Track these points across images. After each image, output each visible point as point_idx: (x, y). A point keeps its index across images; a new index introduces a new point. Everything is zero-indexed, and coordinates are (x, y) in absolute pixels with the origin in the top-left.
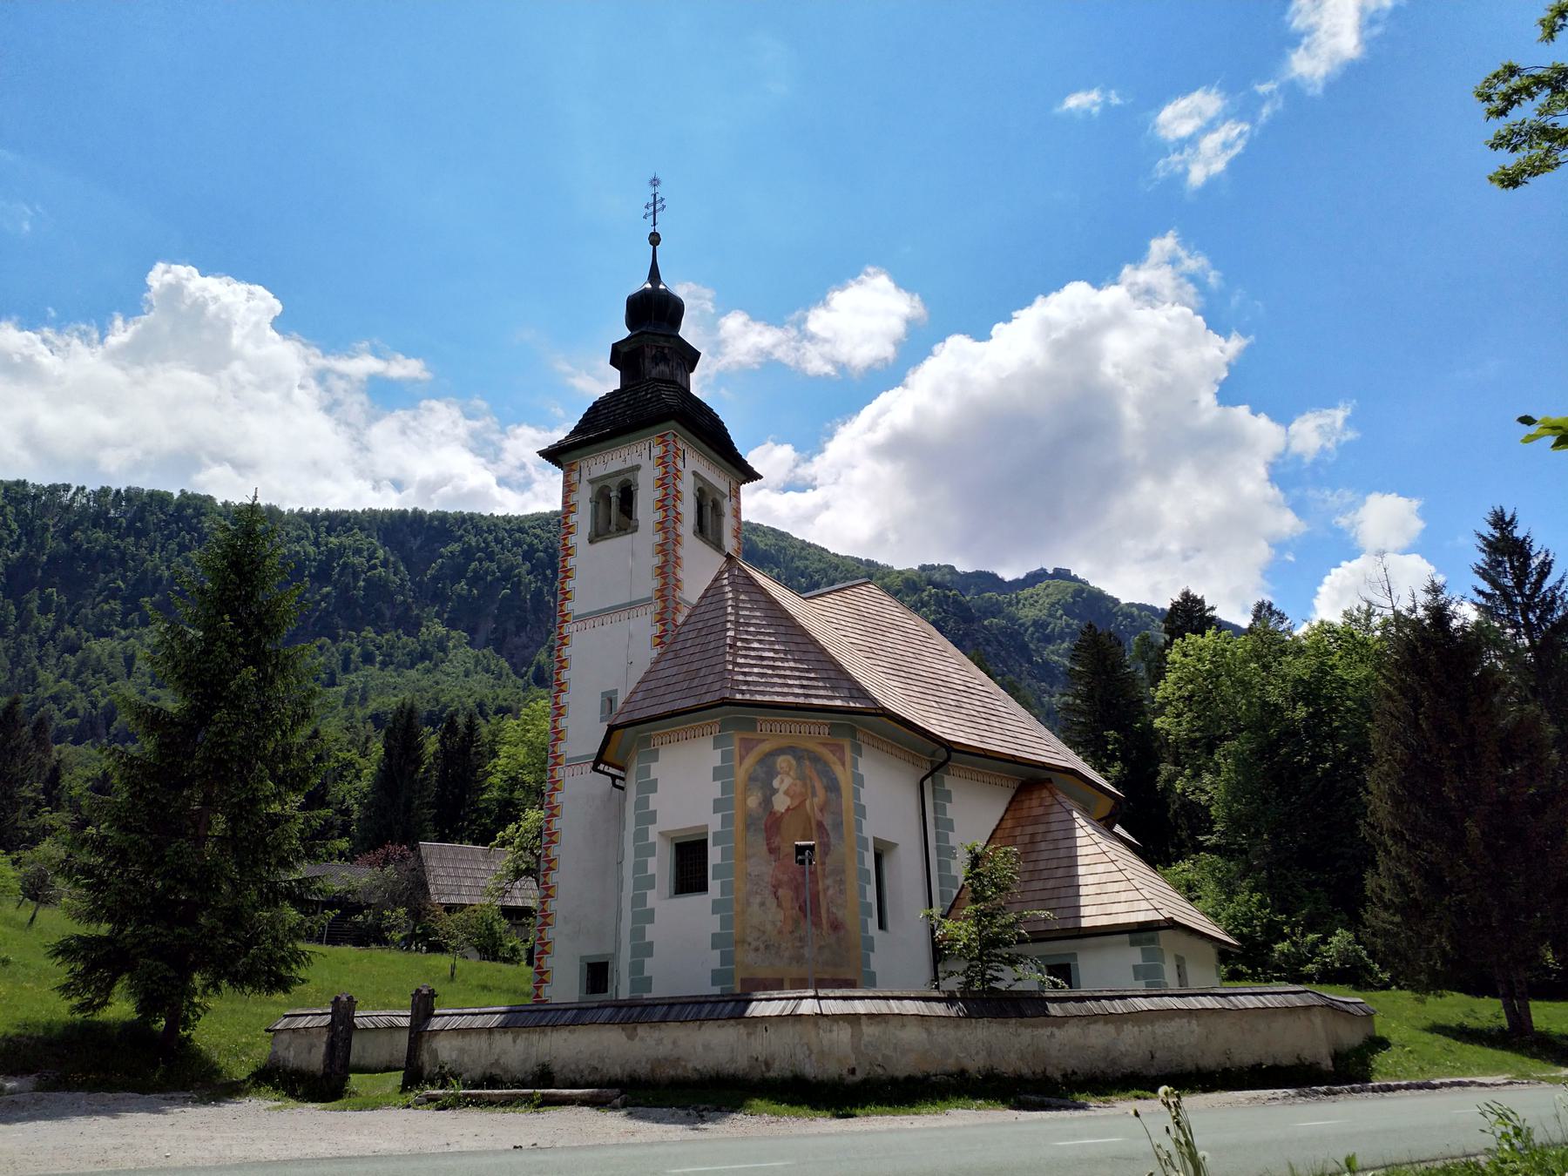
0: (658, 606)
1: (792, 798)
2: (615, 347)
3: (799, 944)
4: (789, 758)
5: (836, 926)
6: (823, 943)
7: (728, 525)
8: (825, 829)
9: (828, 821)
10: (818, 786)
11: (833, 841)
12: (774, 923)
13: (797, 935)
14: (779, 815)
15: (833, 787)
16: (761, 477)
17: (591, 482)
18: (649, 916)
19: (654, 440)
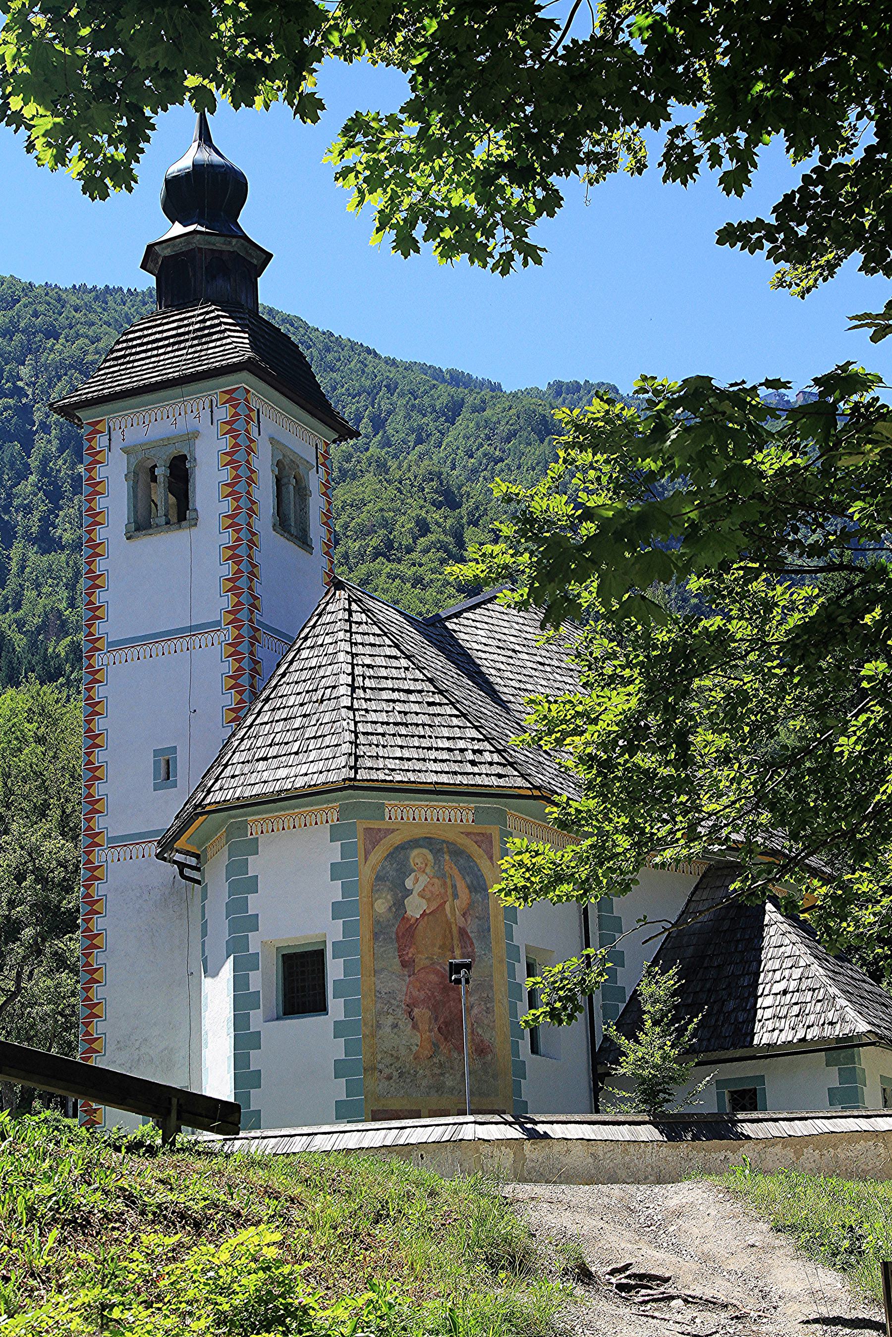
1: (428, 900)
2: (150, 247)
3: (438, 1071)
4: (425, 851)
9: (472, 928)
10: (461, 886)
17: (125, 450)
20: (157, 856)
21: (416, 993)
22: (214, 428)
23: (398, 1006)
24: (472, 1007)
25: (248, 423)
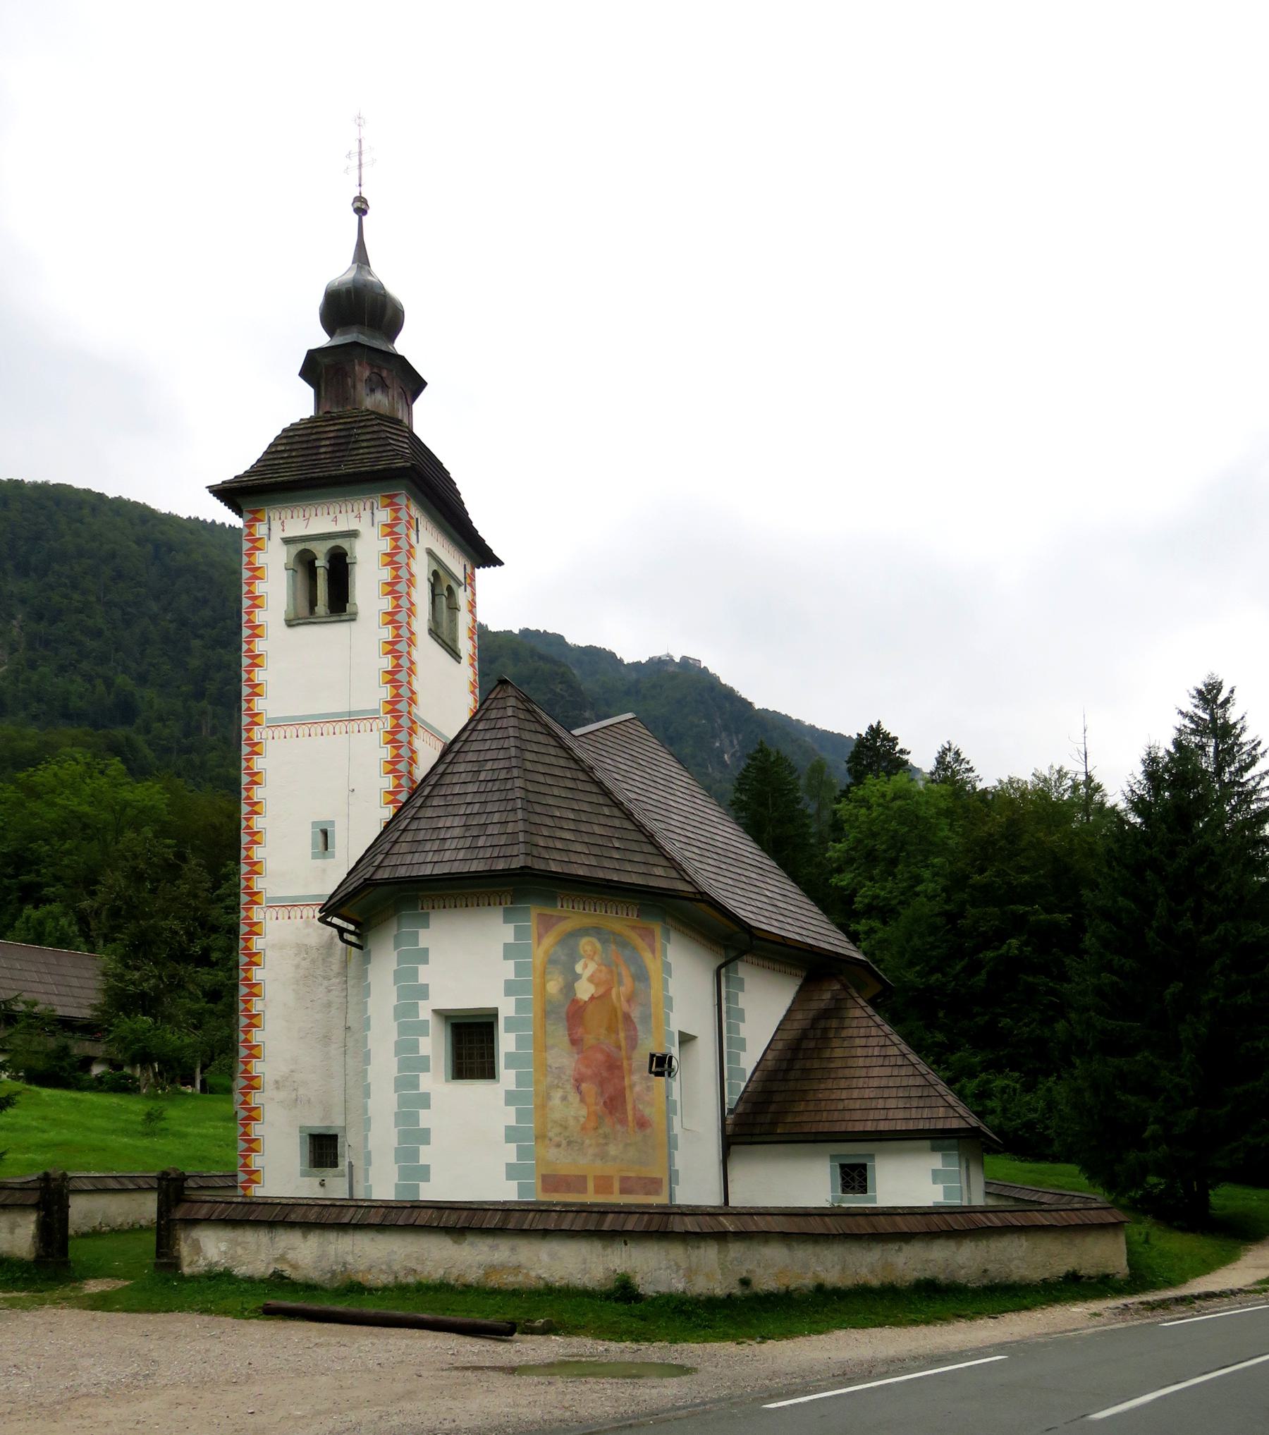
0: (389, 723)
4: (594, 940)
5: (642, 1124)
7: (464, 619)
8: (632, 1021)
9: (635, 1014)
11: (641, 1034)
12: (576, 1118)
13: (601, 1131)
14: (581, 1004)
15: (641, 976)
16: (500, 563)
18: (425, 1101)
19: (378, 500)
20: (319, 919)
21: (583, 1070)
23: (567, 1080)
25: (408, 529)
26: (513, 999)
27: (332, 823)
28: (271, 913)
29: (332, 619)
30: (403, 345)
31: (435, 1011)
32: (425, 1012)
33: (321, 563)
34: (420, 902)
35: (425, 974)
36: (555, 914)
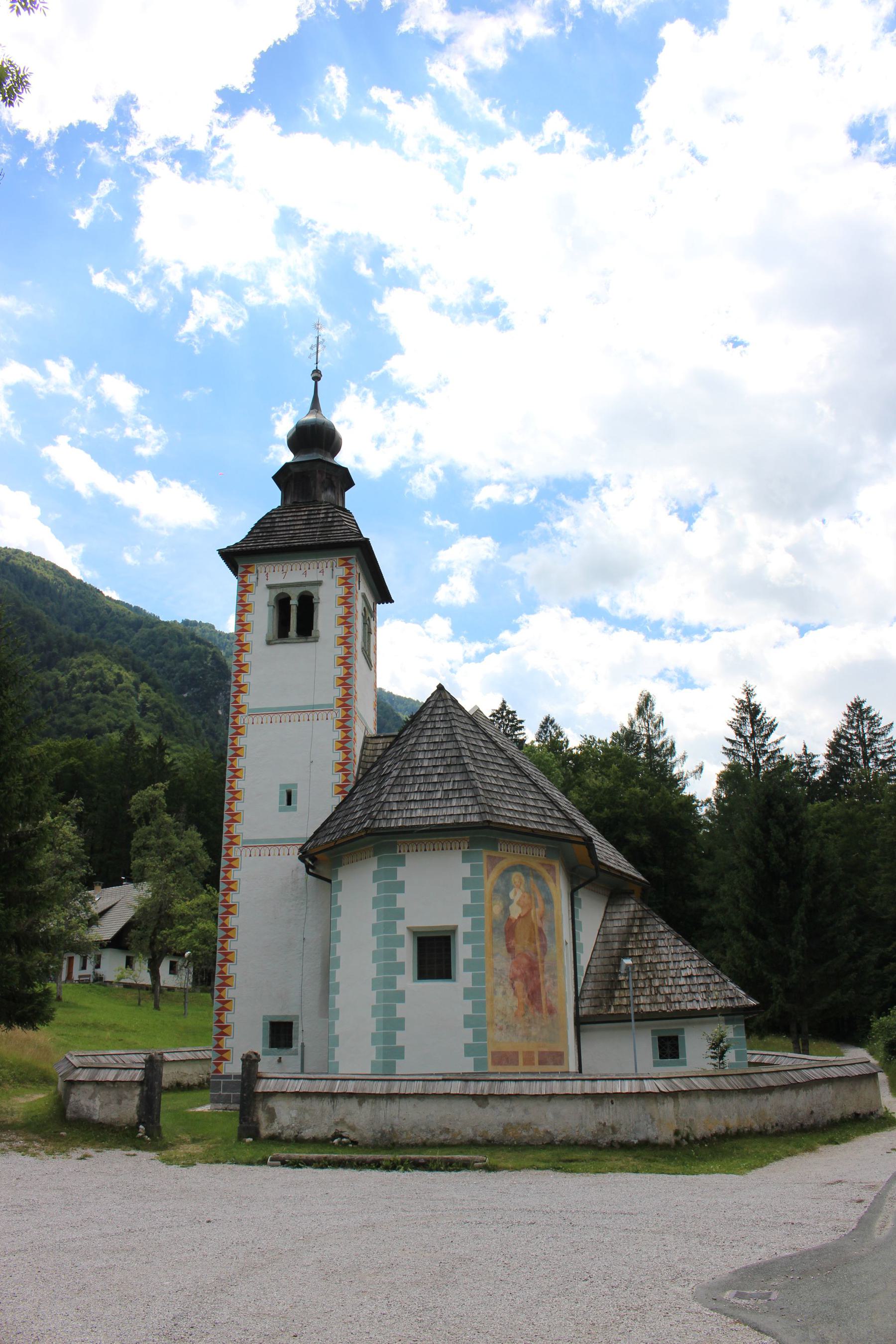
0: (341, 713)
3: (528, 1025)
4: (520, 874)
6: (543, 1024)
8: (544, 935)
9: (545, 929)
11: (549, 944)
12: (512, 1008)
19: (337, 560)
22: (334, 581)
24: (546, 981)
26: (469, 919)
27: (295, 785)
28: (246, 851)
29: (301, 640)
30: (342, 459)
31: (408, 928)
32: (401, 929)
33: (294, 602)
34: (398, 846)
35: (401, 900)
36: (496, 855)
